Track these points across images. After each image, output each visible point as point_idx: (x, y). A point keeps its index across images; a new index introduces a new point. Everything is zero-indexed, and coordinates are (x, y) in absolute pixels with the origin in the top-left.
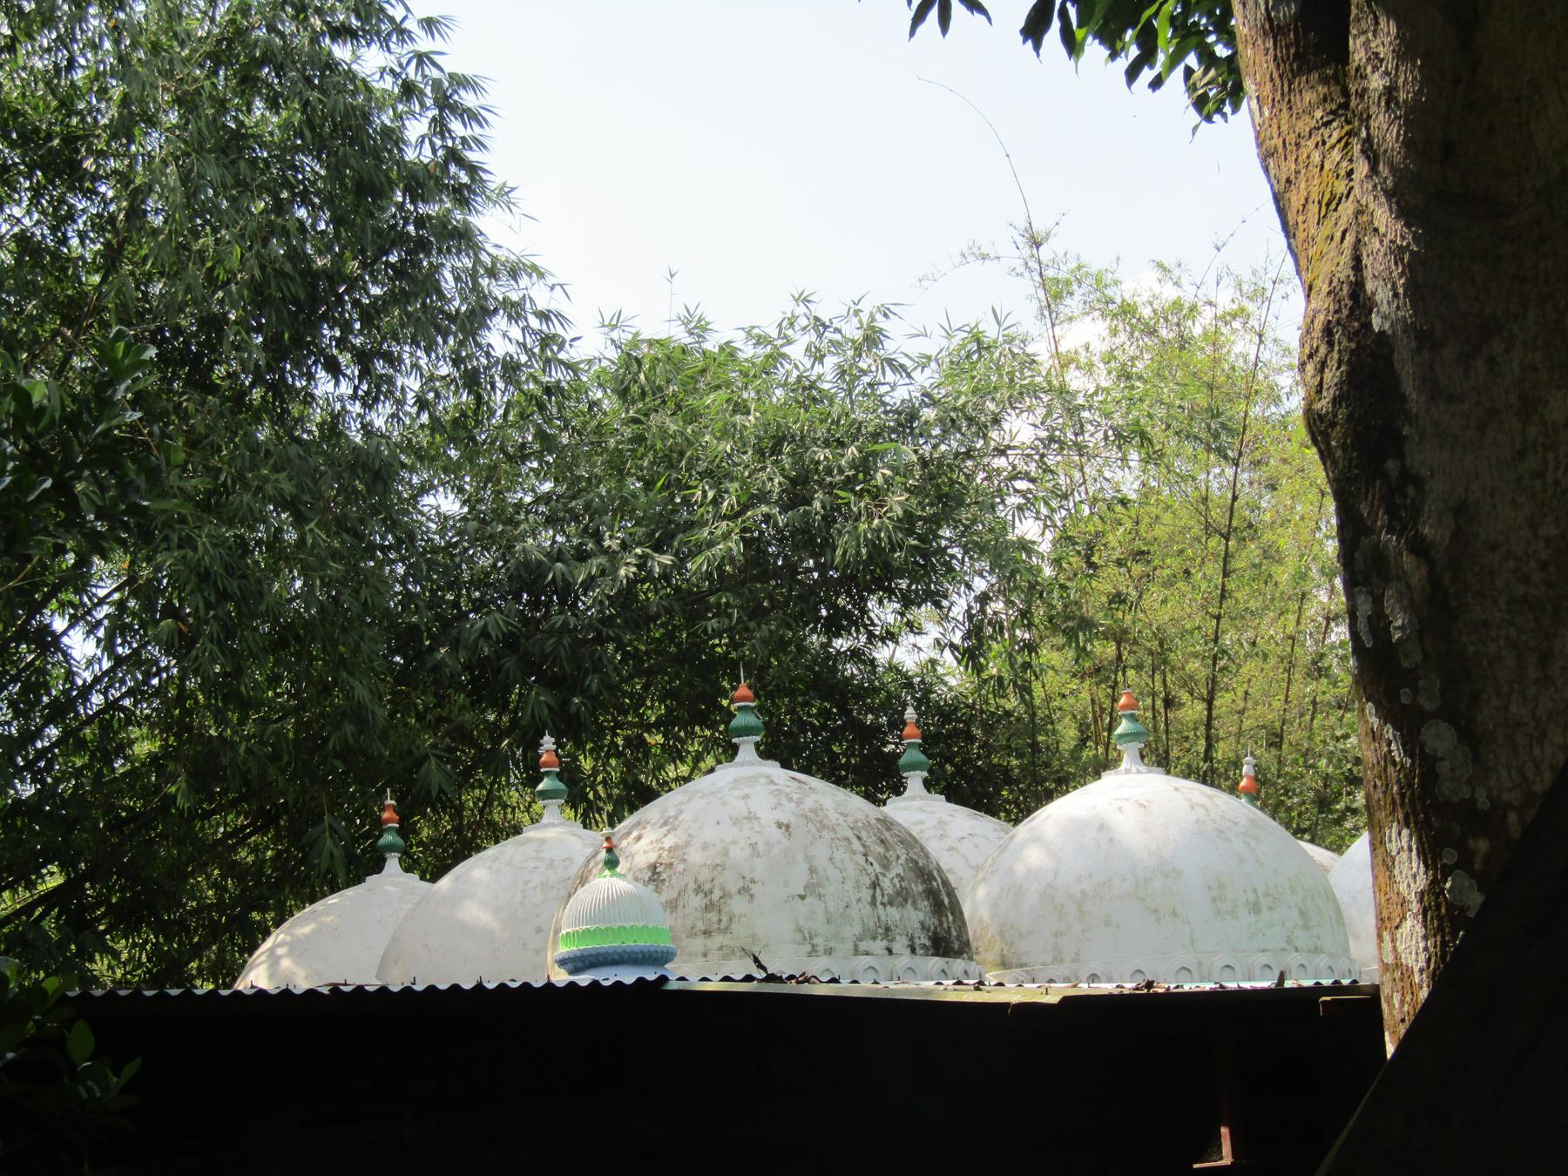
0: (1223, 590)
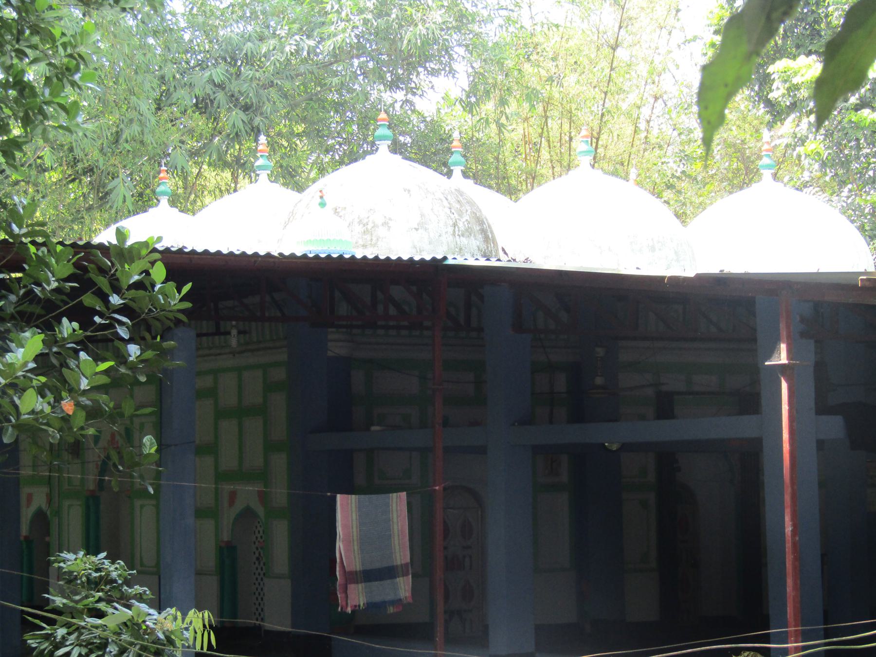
0: (610, 77)
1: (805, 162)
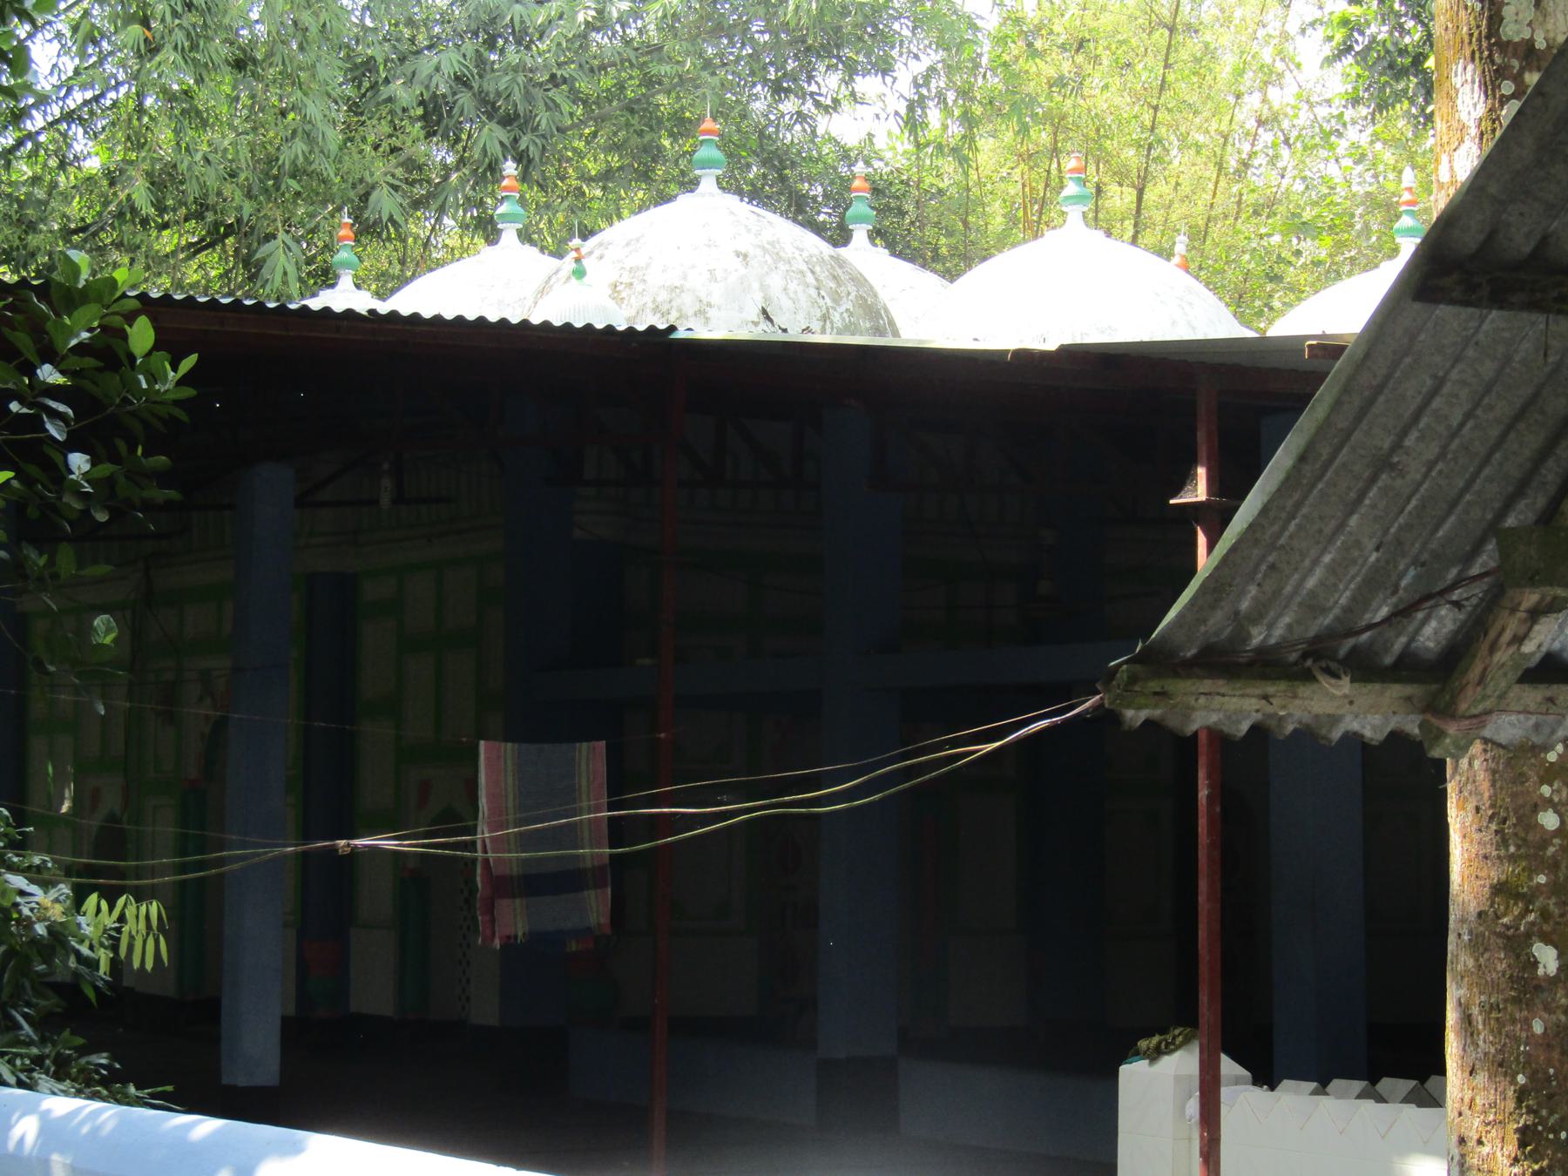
0: (1163, 81)
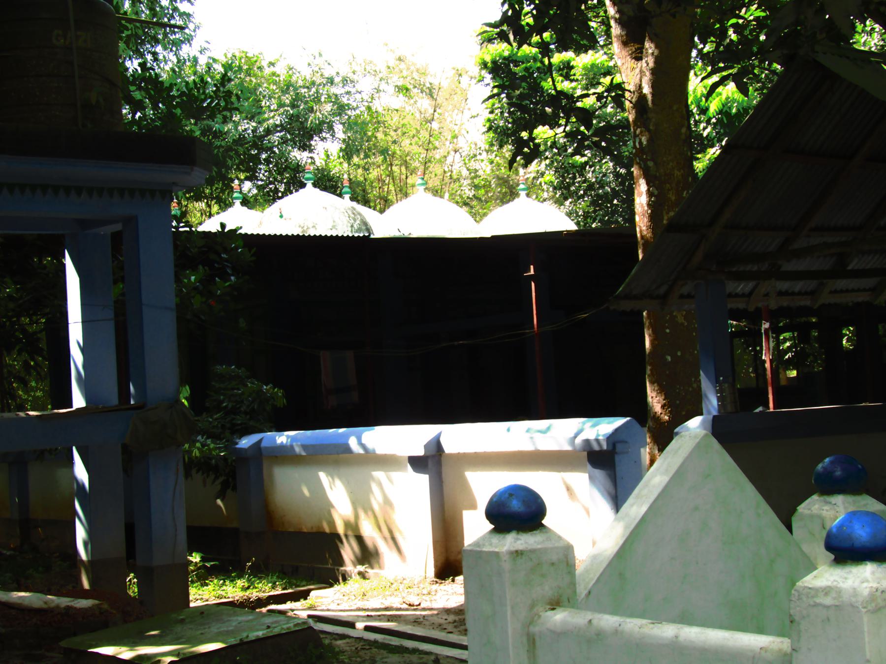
1: (545, 187)
